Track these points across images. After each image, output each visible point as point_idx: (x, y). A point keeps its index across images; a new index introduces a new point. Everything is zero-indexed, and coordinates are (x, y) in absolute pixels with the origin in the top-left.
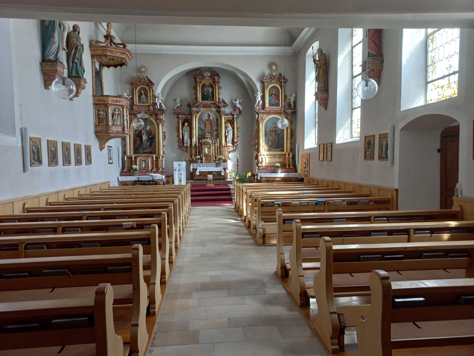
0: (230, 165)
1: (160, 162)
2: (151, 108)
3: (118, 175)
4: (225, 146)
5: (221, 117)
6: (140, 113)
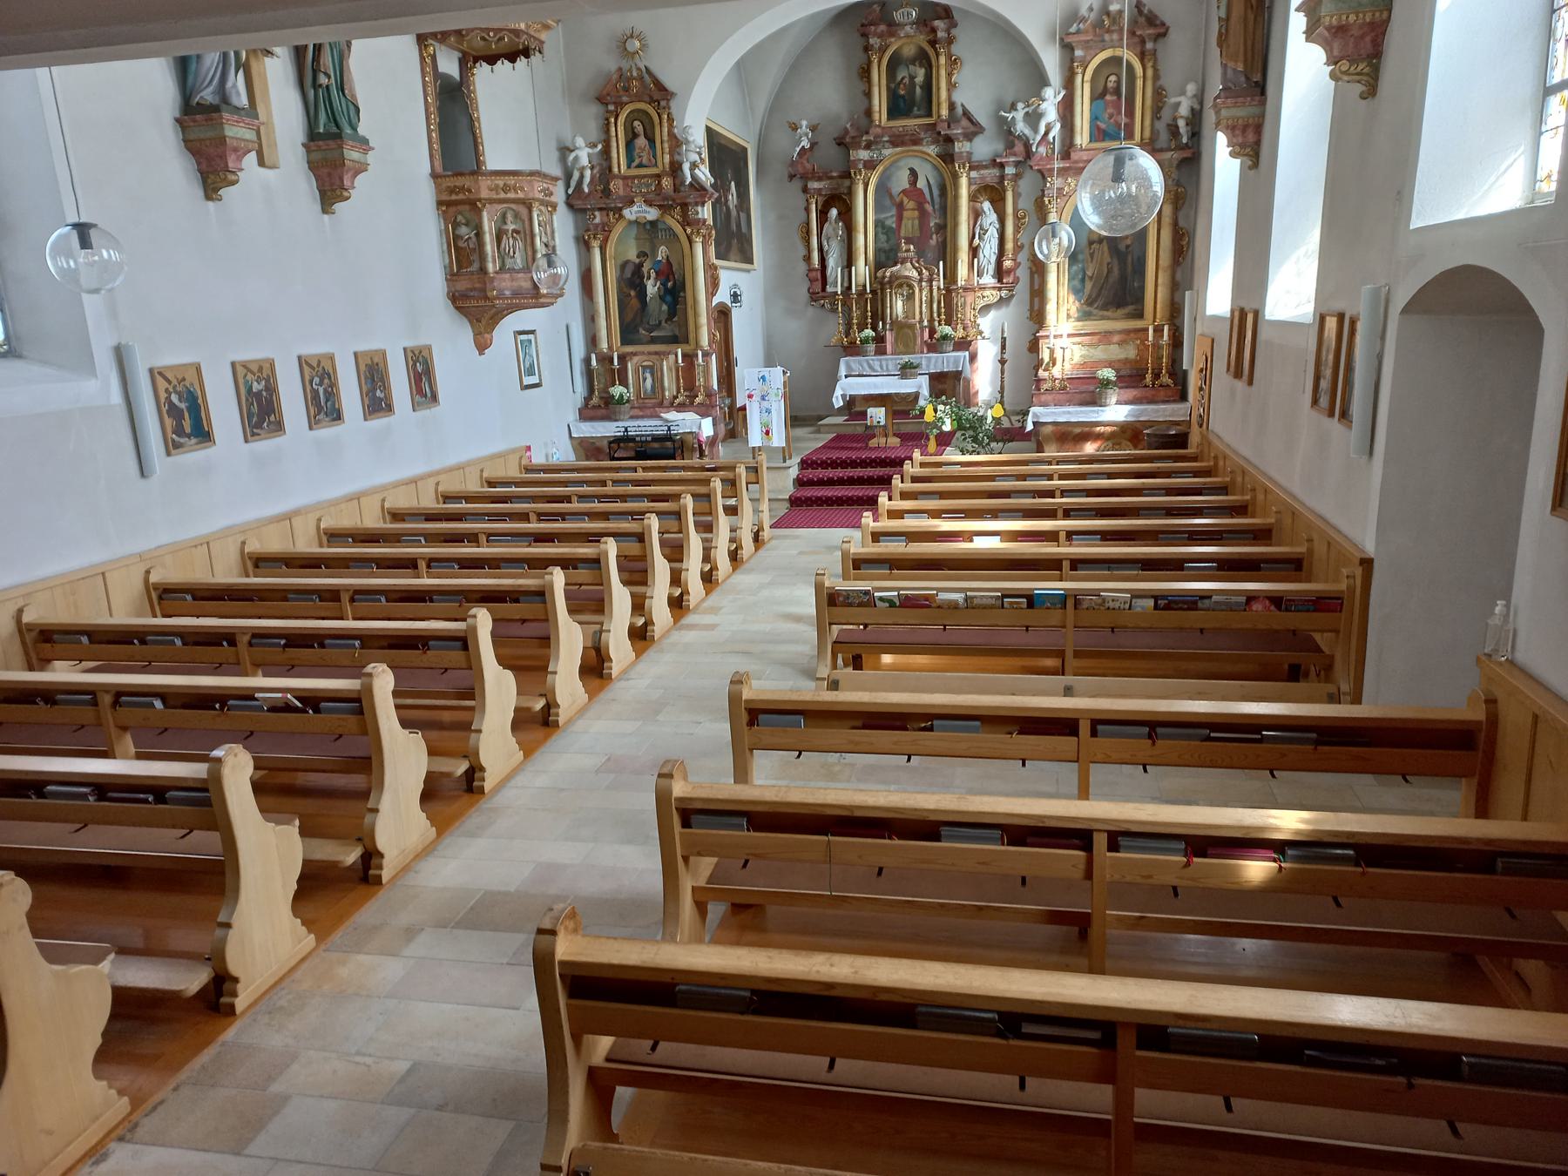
0: (987, 352)
1: (699, 371)
2: (666, 182)
3: (572, 416)
4: (965, 289)
5: (955, 177)
6: (632, 203)
